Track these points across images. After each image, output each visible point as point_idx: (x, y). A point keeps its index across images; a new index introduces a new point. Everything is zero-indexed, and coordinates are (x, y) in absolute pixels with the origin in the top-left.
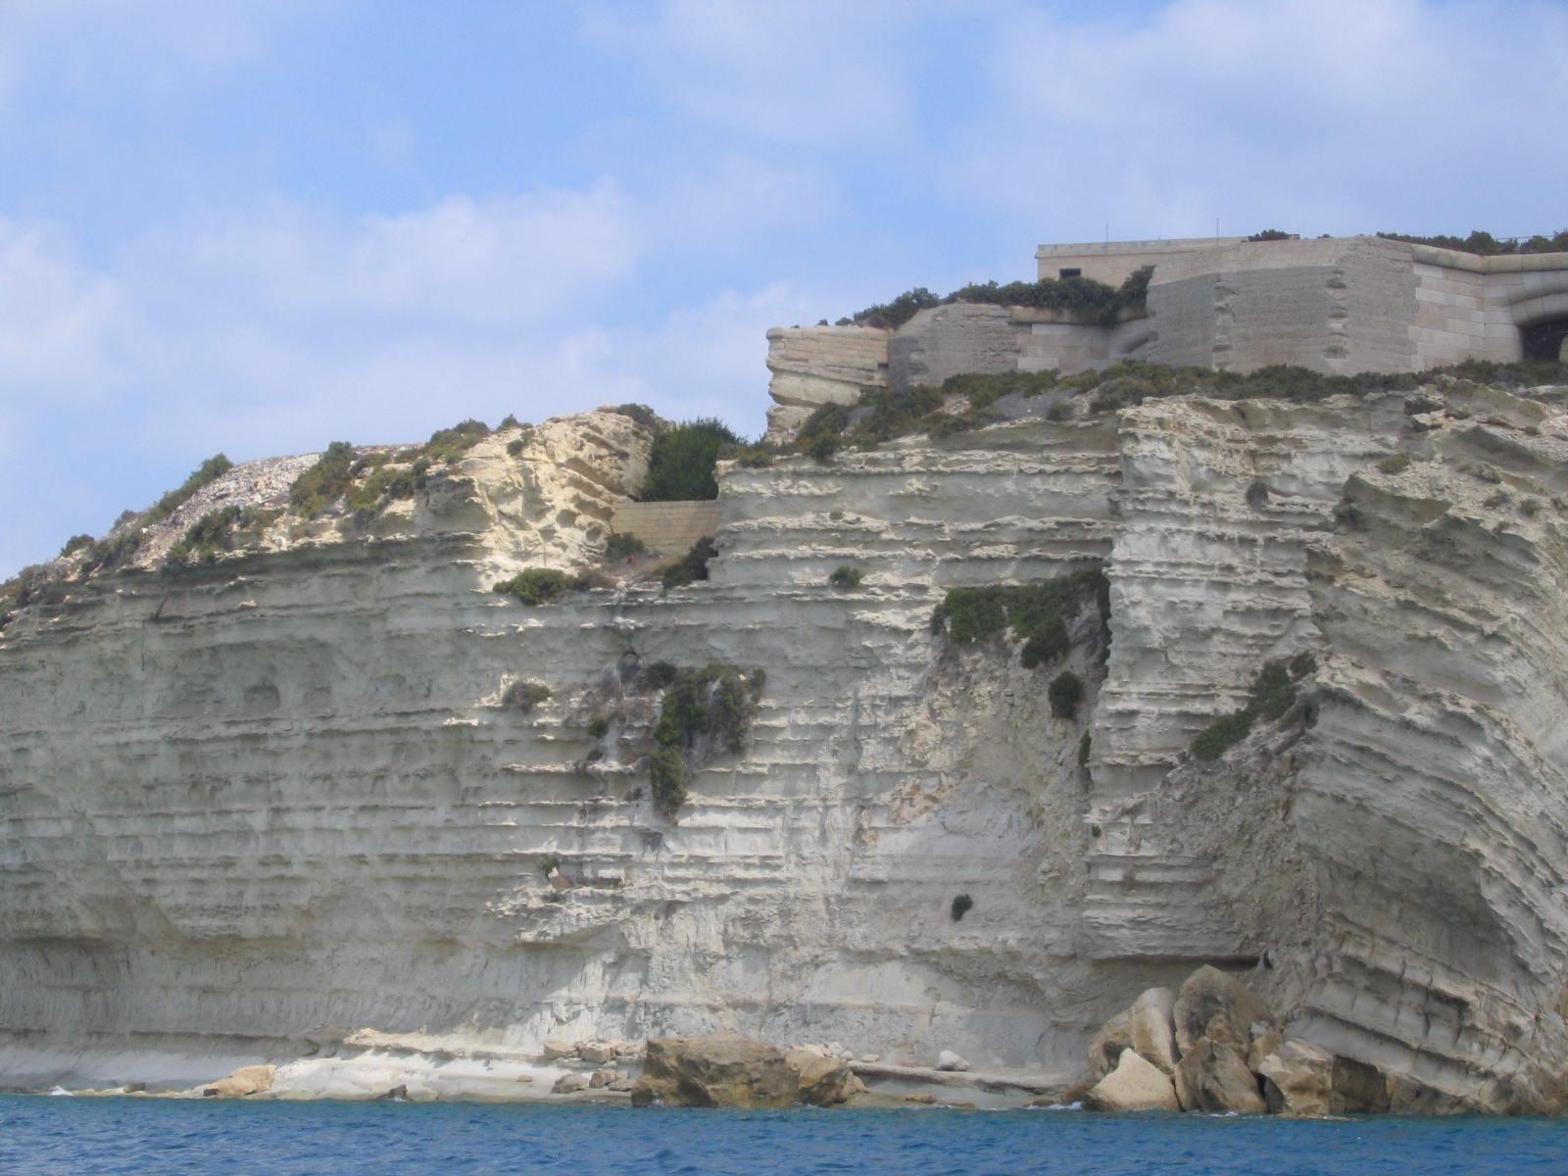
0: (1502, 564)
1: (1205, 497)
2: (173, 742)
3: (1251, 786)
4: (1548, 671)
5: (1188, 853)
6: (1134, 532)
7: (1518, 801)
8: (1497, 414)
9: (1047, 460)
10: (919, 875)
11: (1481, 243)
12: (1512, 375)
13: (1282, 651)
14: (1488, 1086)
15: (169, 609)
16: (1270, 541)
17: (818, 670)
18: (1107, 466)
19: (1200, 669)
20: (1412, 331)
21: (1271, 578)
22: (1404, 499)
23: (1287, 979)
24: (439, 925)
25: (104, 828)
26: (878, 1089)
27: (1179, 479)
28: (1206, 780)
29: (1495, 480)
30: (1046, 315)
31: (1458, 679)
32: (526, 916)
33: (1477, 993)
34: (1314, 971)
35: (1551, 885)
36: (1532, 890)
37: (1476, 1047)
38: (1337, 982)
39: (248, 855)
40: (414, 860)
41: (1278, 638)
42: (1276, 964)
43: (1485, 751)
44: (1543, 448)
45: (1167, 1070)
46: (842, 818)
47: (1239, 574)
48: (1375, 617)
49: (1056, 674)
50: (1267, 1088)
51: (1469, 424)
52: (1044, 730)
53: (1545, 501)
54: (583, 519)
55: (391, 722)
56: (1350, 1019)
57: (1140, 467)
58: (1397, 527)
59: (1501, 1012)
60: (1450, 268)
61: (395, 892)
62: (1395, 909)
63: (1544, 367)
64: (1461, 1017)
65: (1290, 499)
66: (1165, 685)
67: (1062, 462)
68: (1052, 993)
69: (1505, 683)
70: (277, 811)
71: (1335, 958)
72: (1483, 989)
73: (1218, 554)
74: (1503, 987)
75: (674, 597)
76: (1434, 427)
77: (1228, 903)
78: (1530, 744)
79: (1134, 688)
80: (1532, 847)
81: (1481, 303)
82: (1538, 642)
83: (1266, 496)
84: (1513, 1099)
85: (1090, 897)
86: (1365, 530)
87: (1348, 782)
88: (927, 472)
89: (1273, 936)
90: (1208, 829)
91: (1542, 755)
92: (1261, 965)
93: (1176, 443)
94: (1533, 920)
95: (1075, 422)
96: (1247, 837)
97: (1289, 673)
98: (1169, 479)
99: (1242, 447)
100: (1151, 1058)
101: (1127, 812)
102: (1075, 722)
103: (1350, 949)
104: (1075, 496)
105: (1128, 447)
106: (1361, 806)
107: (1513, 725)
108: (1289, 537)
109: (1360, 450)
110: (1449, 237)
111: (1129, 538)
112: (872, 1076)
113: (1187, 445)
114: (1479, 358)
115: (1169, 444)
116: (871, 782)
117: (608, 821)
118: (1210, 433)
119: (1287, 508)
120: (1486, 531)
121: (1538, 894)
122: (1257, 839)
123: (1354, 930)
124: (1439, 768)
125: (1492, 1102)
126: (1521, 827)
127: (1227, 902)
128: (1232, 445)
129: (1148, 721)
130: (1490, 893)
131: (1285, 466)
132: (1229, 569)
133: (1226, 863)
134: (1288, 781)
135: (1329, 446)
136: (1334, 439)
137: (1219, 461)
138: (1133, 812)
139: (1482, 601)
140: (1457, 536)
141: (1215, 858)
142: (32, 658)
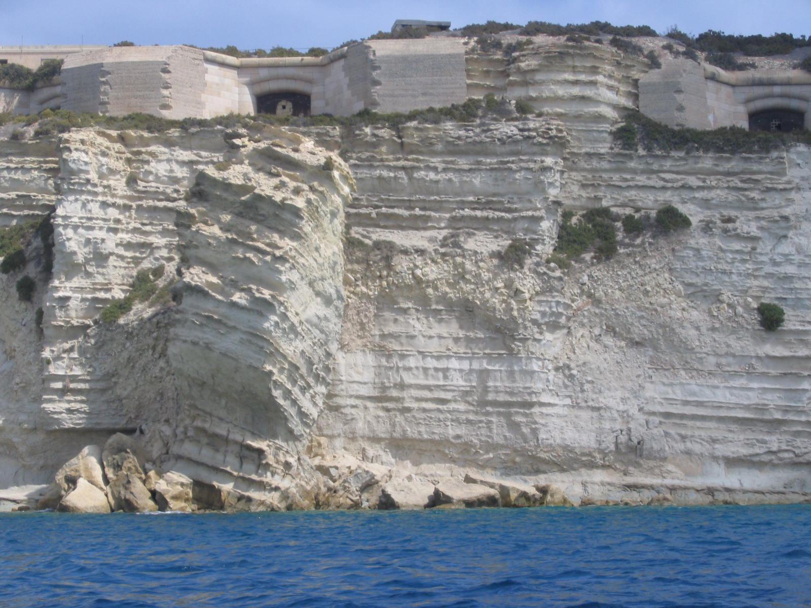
0: (283, 219)
1: (105, 183)
3: (134, 337)
4: (307, 276)
6: (68, 201)
7: (290, 344)
8: (277, 141)
9: (11, 161)
13: (146, 265)
14: (276, 495)
16: (139, 207)
18: (44, 165)
19: (103, 274)
21: (140, 226)
22: (230, 185)
23: (153, 440)
27: (91, 172)
28: (109, 334)
29: (277, 175)
33: (268, 446)
34: (176, 435)
35: (305, 388)
36: (296, 391)
37: (269, 474)
38: (190, 441)
41: (144, 258)
42: (147, 431)
43: (276, 318)
44: (304, 158)
45: (101, 489)
47: (123, 224)
48: (214, 247)
49: (20, 277)
50: (157, 497)
51: (262, 145)
52: (14, 307)
56: (199, 460)
58: (226, 199)
59: (281, 455)
60: (222, 64)
62: (223, 402)
64: (260, 459)
65: (149, 184)
67: (18, 163)
68: (22, 449)
69: (286, 282)
71: (190, 428)
72: (271, 444)
73: (113, 213)
76: (244, 146)
77: (120, 400)
78: (297, 314)
79: (68, 284)
82: (301, 260)
83: (137, 182)
84: (289, 501)
85: (45, 397)
86: (207, 201)
87: (200, 335)
89: (144, 417)
90: (110, 360)
91: (303, 320)
92: (138, 432)
93: (90, 153)
95: (26, 141)
96: (132, 364)
97: (151, 277)
98: (87, 172)
99: (124, 156)
101: (65, 351)
102: (32, 302)
103: (198, 423)
104: (26, 181)
105: (65, 155)
106: (208, 347)
107: (289, 304)
108: (149, 204)
109: (186, 159)
110: (726, 34)
111: (65, 203)
113: (95, 154)
115: (87, 153)
118: (107, 148)
119: (148, 189)
120: (276, 202)
121: (299, 393)
122: (137, 365)
123: (201, 413)
124: (250, 327)
125: (279, 503)
126: (292, 358)
127: (120, 400)
128: (118, 155)
129: (76, 302)
130: (277, 393)
131: (146, 167)
132: (118, 221)
133: (118, 378)
134: (155, 335)
135: (170, 156)
136: (172, 153)
139: (274, 239)
141: (113, 376)
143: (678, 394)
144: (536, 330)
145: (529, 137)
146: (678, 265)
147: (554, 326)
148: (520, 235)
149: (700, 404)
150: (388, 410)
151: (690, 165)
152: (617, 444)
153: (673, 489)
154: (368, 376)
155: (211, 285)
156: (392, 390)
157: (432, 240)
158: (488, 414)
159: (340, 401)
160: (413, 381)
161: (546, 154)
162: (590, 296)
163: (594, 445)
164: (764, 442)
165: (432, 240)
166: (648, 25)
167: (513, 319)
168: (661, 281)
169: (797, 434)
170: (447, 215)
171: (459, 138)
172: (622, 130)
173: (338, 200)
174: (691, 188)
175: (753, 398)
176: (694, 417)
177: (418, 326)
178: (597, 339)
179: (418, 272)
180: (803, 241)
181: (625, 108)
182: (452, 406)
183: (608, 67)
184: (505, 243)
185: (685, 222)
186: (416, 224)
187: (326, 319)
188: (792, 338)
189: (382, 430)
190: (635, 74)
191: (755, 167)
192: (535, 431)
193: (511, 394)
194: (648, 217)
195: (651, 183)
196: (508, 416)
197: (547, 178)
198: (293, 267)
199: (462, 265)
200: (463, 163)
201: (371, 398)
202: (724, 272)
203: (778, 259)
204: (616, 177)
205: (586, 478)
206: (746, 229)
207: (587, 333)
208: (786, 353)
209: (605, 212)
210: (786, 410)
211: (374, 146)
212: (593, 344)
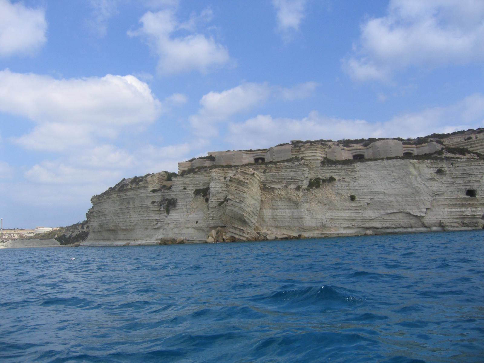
2: (120, 209)
5: (218, 216)
8: (245, 169)
10: (193, 219)
11: (251, 151)
12: (254, 164)
14: (246, 238)
15: (119, 195)
17: (182, 198)
20: (243, 160)
24: (146, 227)
25: (114, 218)
26: (188, 241)
30: (207, 160)
31: (241, 197)
32: (154, 225)
36: (250, 218)
39: (128, 220)
40: (144, 220)
46: (185, 213)
49: (205, 198)
53: (249, 178)
54: (160, 183)
55: (141, 206)
57: (212, 176)
60: (246, 153)
61: (142, 223)
63: (257, 163)
66: (216, 198)
68: (206, 231)
70: (130, 215)
73: (220, 184)
74: (248, 228)
75: (168, 191)
80: (250, 214)
81: (250, 157)
88: (193, 177)
94: (6, 229)
100: (213, 237)
106: (232, 210)
110: (360, 139)
112: (188, 240)
114: (250, 162)
116: (188, 210)
117: (162, 215)
127: (223, 220)
130: (245, 218)
132: (222, 186)
137: (221, 175)
138: (213, 212)
140: (241, 182)
142: (106, 200)
143: (334, 214)
144: (302, 203)
145: (301, 165)
146: (333, 188)
147: (307, 202)
148: (299, 184)
149: (338, 216)
150: (274, 220)
151: (336, 168)
152: (320, 225)
153: (331, 234)
154: (270, 214)
155: (232, 198)
156: (72, 234)
157: (282, 186)
158: (294, 220)
159: (265, 219)
160: (279, 215)
161: (304, 168)
162: (315, 196)
163: (315, 226)
164: (351, 224)
165: (282, 186)
166: (331, 139)
167: (298, 201)
168: (330, 192)
169: (358, 221)
170: (286, 181)
171: (287, 166)
172: (322, 161)
173: (257, 180)
174: (336, 172)
175: (349, 215)
176: (337, 219)
177: (280, 204)
178: (317, 204)
179: (279, 193)
180: (360, 182)
181: (324, 157)
182: (287, 219)
183: (319, 149)
184: (296, 186)
185: (335, 179)
186: (280, 183)
187: (256, 204)
188: (357, 202)
189: (273, 224)
190: (326, 150)
191: (349, 167)
192: (303, 223)
193: (298, 216)
194: (327, 179)
195: (328, 172)
196: (298, 220)
197: (305, 172)
198: (247, 194)
199: (288, 191)
200: (289, 170)
201: (271, 218)
202: (343, 189)
203: (354, 186)
204: (321, 171)
205: (314, 232)
206: (347, 180)
207: (314, 203)
208: (356, 205)
209: (319, 178)
210: (356, 217)
211: (271, 168)
212: (315, 205)
